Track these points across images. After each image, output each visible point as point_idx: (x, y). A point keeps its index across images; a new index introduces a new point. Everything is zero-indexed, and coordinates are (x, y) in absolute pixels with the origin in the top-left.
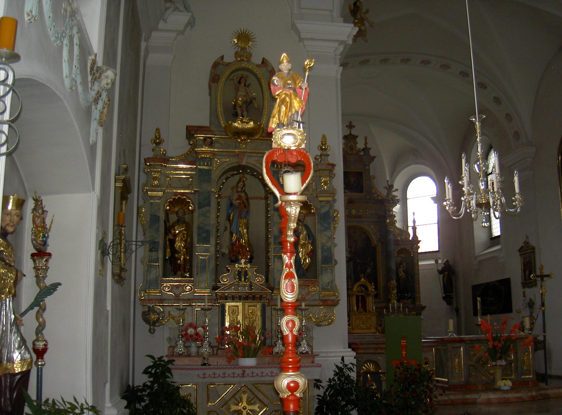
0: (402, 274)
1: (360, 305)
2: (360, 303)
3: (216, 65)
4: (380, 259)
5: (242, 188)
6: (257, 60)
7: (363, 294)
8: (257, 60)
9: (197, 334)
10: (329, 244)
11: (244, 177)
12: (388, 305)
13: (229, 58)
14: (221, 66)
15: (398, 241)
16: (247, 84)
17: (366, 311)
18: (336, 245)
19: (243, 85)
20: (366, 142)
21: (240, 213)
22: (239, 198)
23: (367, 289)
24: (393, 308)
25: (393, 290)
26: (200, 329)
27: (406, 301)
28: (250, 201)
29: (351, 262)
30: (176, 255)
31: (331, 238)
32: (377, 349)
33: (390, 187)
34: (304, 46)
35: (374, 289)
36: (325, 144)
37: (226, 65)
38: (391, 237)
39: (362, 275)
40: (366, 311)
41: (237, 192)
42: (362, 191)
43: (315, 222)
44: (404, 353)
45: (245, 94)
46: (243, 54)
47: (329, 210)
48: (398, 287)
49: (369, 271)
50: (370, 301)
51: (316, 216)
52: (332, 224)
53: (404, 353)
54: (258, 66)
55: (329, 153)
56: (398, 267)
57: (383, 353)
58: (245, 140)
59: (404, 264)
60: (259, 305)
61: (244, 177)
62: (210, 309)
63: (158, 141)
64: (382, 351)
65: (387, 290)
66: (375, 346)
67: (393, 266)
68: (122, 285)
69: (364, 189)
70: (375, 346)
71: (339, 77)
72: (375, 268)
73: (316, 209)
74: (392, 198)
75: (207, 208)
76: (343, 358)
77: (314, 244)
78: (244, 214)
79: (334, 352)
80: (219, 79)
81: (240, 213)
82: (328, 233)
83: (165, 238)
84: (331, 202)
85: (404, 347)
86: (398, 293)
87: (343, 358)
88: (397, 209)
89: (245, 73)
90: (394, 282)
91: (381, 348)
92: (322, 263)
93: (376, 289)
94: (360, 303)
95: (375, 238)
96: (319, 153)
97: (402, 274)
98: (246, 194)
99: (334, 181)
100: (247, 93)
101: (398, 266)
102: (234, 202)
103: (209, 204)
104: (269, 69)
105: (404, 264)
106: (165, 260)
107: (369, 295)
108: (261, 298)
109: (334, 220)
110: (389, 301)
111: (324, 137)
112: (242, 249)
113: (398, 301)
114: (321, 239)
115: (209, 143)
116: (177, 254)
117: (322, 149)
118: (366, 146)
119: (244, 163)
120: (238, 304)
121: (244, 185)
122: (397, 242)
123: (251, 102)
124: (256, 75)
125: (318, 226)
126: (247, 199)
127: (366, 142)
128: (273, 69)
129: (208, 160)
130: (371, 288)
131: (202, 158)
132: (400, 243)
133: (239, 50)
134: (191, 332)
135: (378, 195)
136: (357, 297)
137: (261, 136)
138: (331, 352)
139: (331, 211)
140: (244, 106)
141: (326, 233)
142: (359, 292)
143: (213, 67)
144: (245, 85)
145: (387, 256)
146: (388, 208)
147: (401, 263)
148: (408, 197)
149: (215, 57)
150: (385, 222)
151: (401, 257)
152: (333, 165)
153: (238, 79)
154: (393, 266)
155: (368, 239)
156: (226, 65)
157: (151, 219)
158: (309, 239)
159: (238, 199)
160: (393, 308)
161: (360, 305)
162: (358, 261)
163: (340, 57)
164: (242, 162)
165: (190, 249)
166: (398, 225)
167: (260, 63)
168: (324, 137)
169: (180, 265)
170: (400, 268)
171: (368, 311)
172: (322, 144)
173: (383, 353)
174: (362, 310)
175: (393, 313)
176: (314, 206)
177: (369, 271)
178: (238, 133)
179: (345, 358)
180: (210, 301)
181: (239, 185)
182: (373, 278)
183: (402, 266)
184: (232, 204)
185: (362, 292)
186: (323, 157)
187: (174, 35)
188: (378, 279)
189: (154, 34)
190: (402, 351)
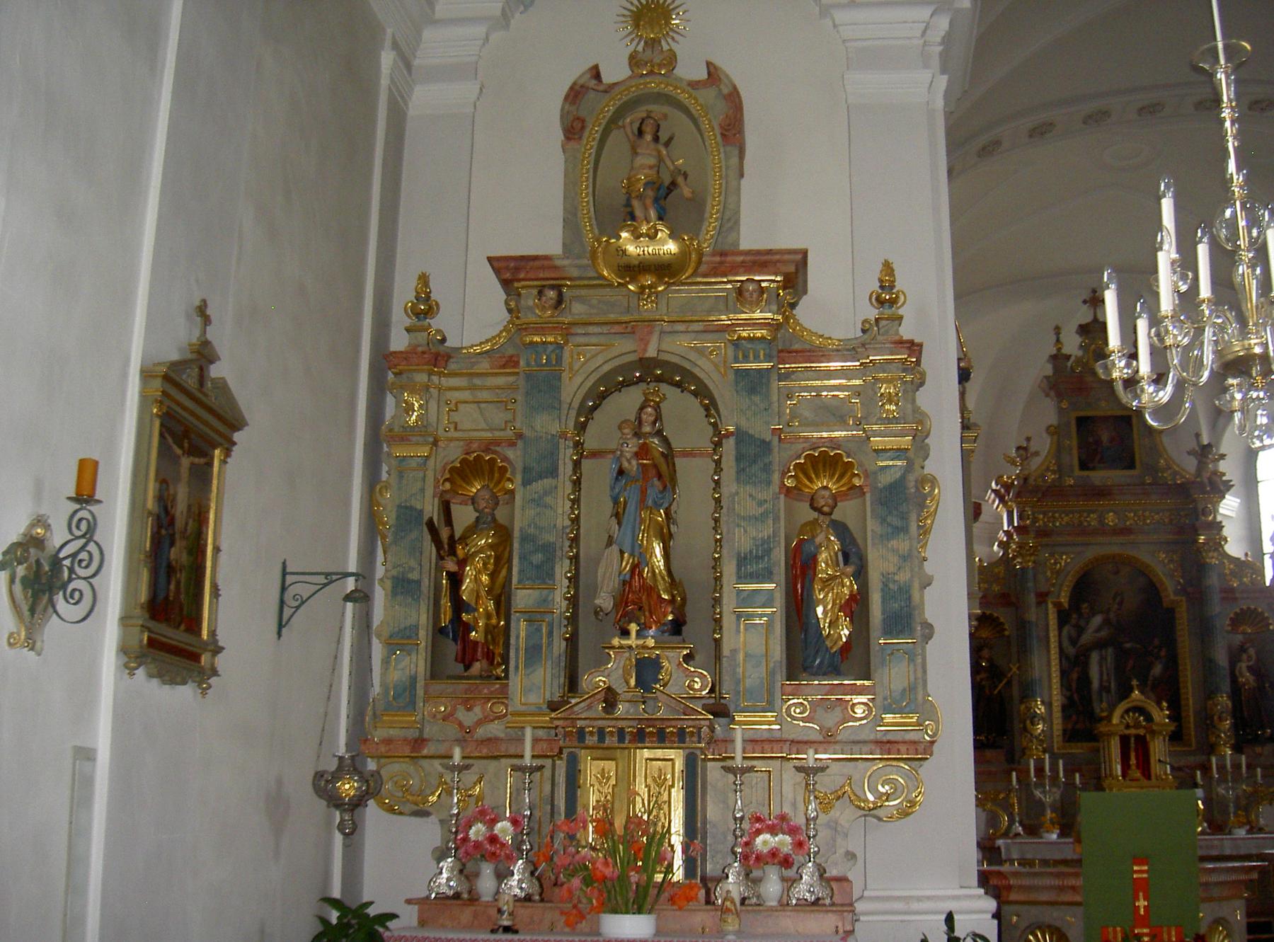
0: (1247, 678)
1: (1133, 761)
2: (1133, 755)
3: (575, 94)
4: (1186, 642)
5: (654, 423)
6: (690, 69)
7: (1142, 732)
8: (690, 69)
9: (493, 839)
10: (902, 577)
11: (656, 393)
12: (1209, 761)
13: (616, 71)
14: (592, 95)
15: (1232, 590)
16: (664, 136)
17: (1148, 777)
18: (927, 583)
19: (649, 137)
20: (1058, 340)
21: (643, 492)
22: (643, 451)
23: (1149, 718)
24: (1222, 768)
25: (1220, 719)
26: (504, 828)
27: (1258, 749)
28: (679, 462)
29: (1110, 650)
30: (465, 617)
31: (914, 559)
32: (1061, 889)
33: (1205, 453)
34: (835, 26)
35: (1169, 717)
36: (892, 287)
37: (606, 92)
38: (1213, 581)
39: (1135, 682)
40: (1148, 777)
41: (637, 435)
42: (1131, 466)
43: (865, 511)
44: (1142, 903)
45: (652, 161)
46: (653, 57)
47: (903, 477)
48: (1237, 712)
49: (1157, 670)
50: (1158, 748)
51: (868, 496)
52: (913, 517)
53: (1142, 903)
54: (694, 85)
55: (901, 312)
56: (1234, 660)
57: (1079, 904)
58: (650, 287)
59: (1252, 651)
60: (677, 757)
61: (656, 393)
62: (823, 769)
63: (424, 308)
64: (1078, 898)
65: (1207, 722)
66: (1057, 882)
67: (1222, 658)
68: (204, 692)
69: (1137, 456)
70: (1057, 882)
71: (940, 103)
72: (1172, 662)
73: (867, 476)
74: (1209, 479)
75: (547, 482)
76: (950, 919)
77: (861, 574)
78: (652, 493)
79: (929, 898)
80: (583, 128)
81: (643, 492)
82: (901, 544)
83: (439, 569)
84: (911, 454)
85: (1140, 886)
86: (1235, 726)
87: (950, 919)
88: (1229, 506)
89: (657, 109)
90: (1224, 700)
91: (1073, 888)
92: (888, 632)
93: (1176, 716)
94: (1133, 755)
95: (1170, 589)
96: (872, 313)
97: (1247, 678)
98: (665, 441)
99: (924, 398)
100: (660, 160)
101: (1235, 655)
102: (626, 464)
103: (553, 472)
104: (725, 91)
105: (1252, 651)
106: (439, 631)
107: (1153, 733)
108: (681, 735)
109: (922, 506)
110: (1212, 749)
111: (888, 268)
112: (649, 595)
113: (1237, 749)
114: (879, 562)
115: (552, 302)
116: (467, 613)
117: (881, 302)
118: (1059, 350)
119: (651, 352)
120: (671, 753)
121: (658, 418)
122: (1229, 594)
123: (674, 184)
124: (686, 111)
125: (871, 524)
126: (669, 456)
127: (1058, 340)
128: (735, 88)
129: (551, 348)
130: (1161, 715)
131: (532, 343)
132: (1237, 595)
133: (640, 48)
134: (477, 832)
135: (1176, 473)
136: (1125, 740)
137: (693, 275)
138: (919, 899)
139: (911, 478)
140: (650, 193)
141: (894, 543)
142: (1128, 727)
143: (566, 98)
144: (656, 139)
145: (1205, 630)
146: (1200, 507)
147: (1242, 649)
148: (1259, 478)
149: (574, 72)
150: (1196, 541)
151: (1244, 633)
152: (914, 348)
153: (636, 125)
154: (1222, 658)
155: (1152, 590)
156: (606, 92)
157: (398, 518)
158: (846, 562)
159: (637, 455)
160: (1222, 768)
161: (1133, 761)
162: (1128, 645)
163: (941, 48)
164: (645, 350)
165: (502, 599)
166: (1235, 547)
167: (703, 75)
168: (888, 268)
169: (476, 643)
170: (1240, 661)
171: (1153, 777)
172: (882, 287)
173: (1079, 904)
174: (1138, 774)
175: (1223, 779)
176: (861, 465)
177: (1157, 670)
178: (633, 269)
179: (956, 917)
180: (749, 747)
181: (644, 417)
182: (1169, 691)
183: (1244, 656)
184: (621, 472)
185: (1137, 725)
186: (883, 323)
187: (480, 30)
188: (1182, 691)
189: (428, 34)
190: (1137, 898)
